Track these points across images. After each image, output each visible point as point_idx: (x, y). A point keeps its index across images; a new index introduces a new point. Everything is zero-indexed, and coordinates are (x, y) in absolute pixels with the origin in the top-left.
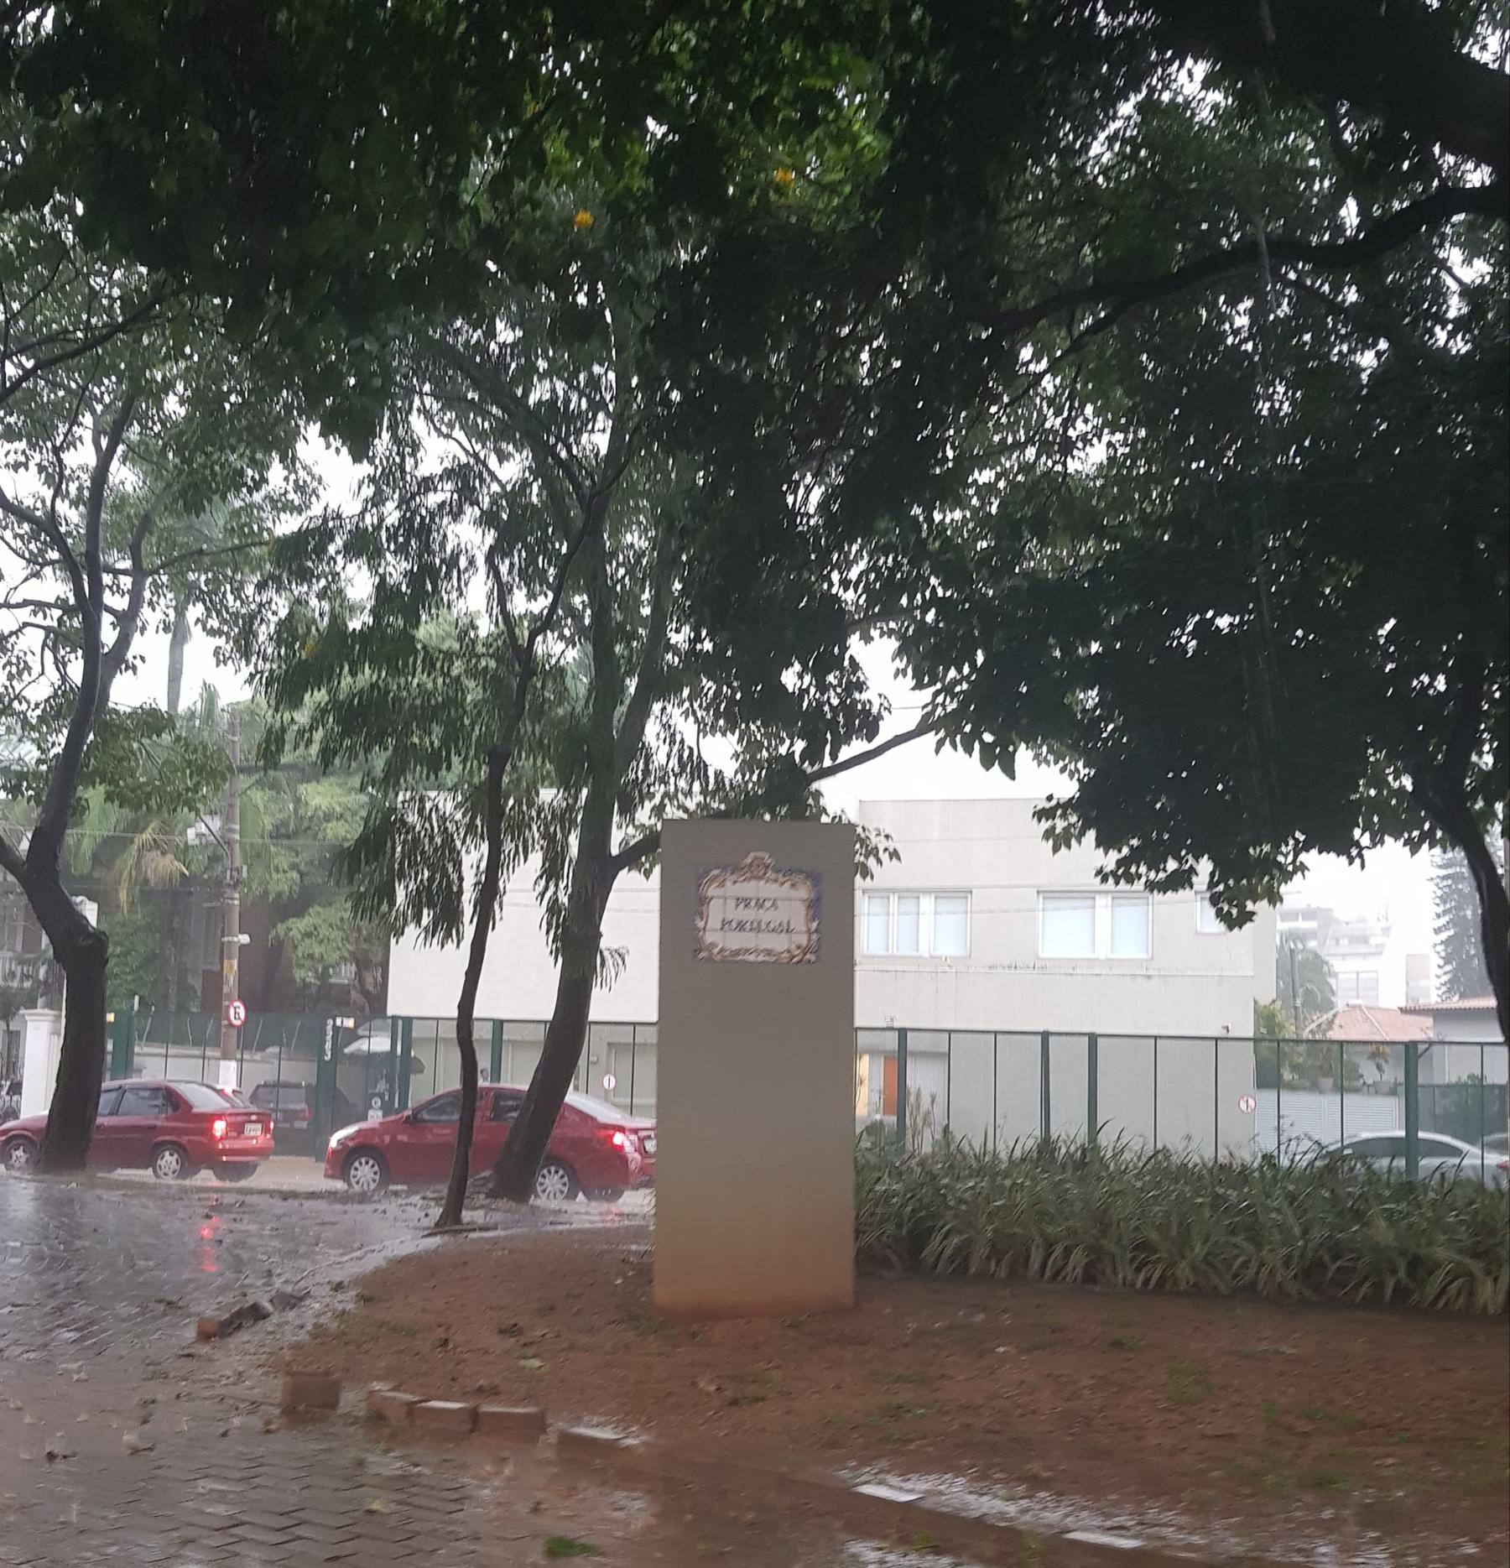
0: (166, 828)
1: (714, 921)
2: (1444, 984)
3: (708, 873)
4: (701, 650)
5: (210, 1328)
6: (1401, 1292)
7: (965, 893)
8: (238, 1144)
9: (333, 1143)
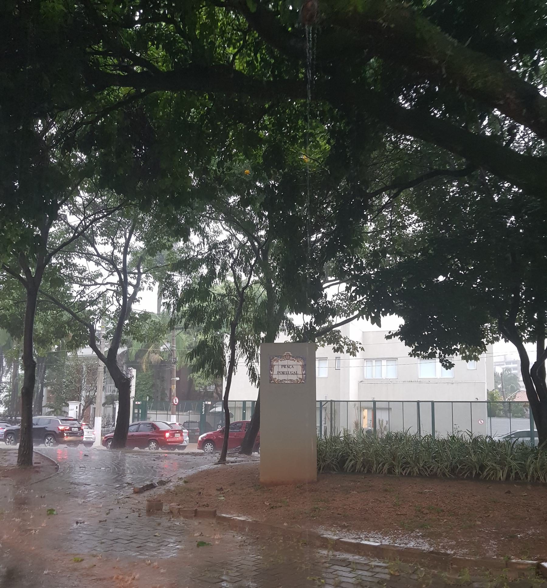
0: (157, 347)
1: (275, 372)
3: (273, 358)
5: (137, 490)
6: (478, 475)
7: (395, 359)
8: (173, 440)
9: (200, 439)
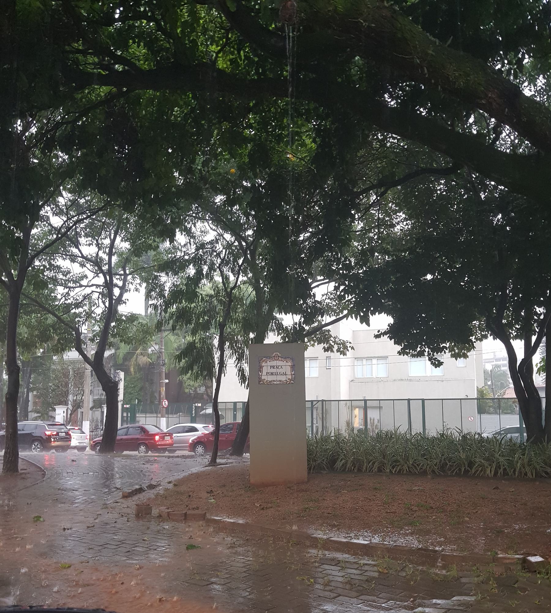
0: (145, 349)
1: (264, 373)
2: (544, 379)
4: (336, 283)
5: (126, 495)
6: (466, 472)
7: (386, 358)
8: (163, 443)
